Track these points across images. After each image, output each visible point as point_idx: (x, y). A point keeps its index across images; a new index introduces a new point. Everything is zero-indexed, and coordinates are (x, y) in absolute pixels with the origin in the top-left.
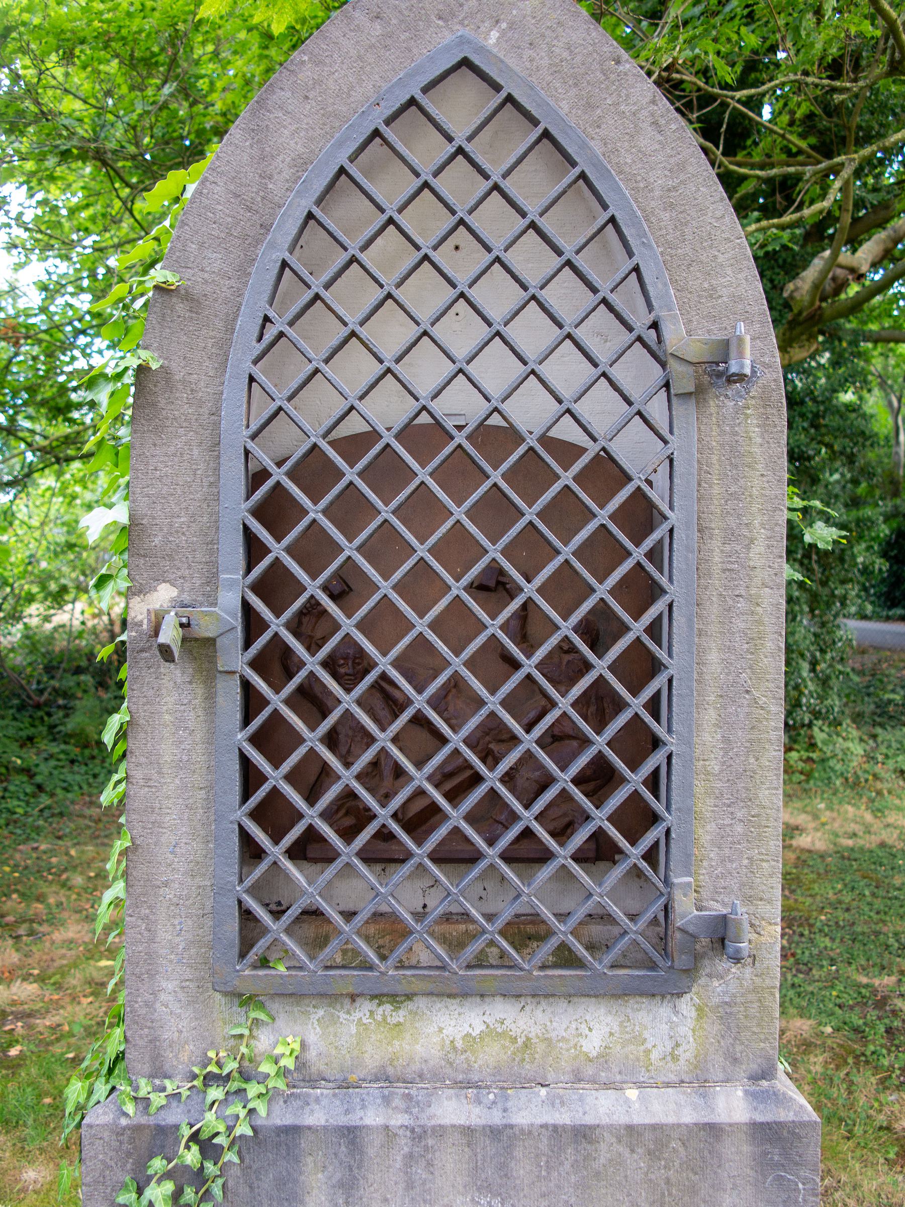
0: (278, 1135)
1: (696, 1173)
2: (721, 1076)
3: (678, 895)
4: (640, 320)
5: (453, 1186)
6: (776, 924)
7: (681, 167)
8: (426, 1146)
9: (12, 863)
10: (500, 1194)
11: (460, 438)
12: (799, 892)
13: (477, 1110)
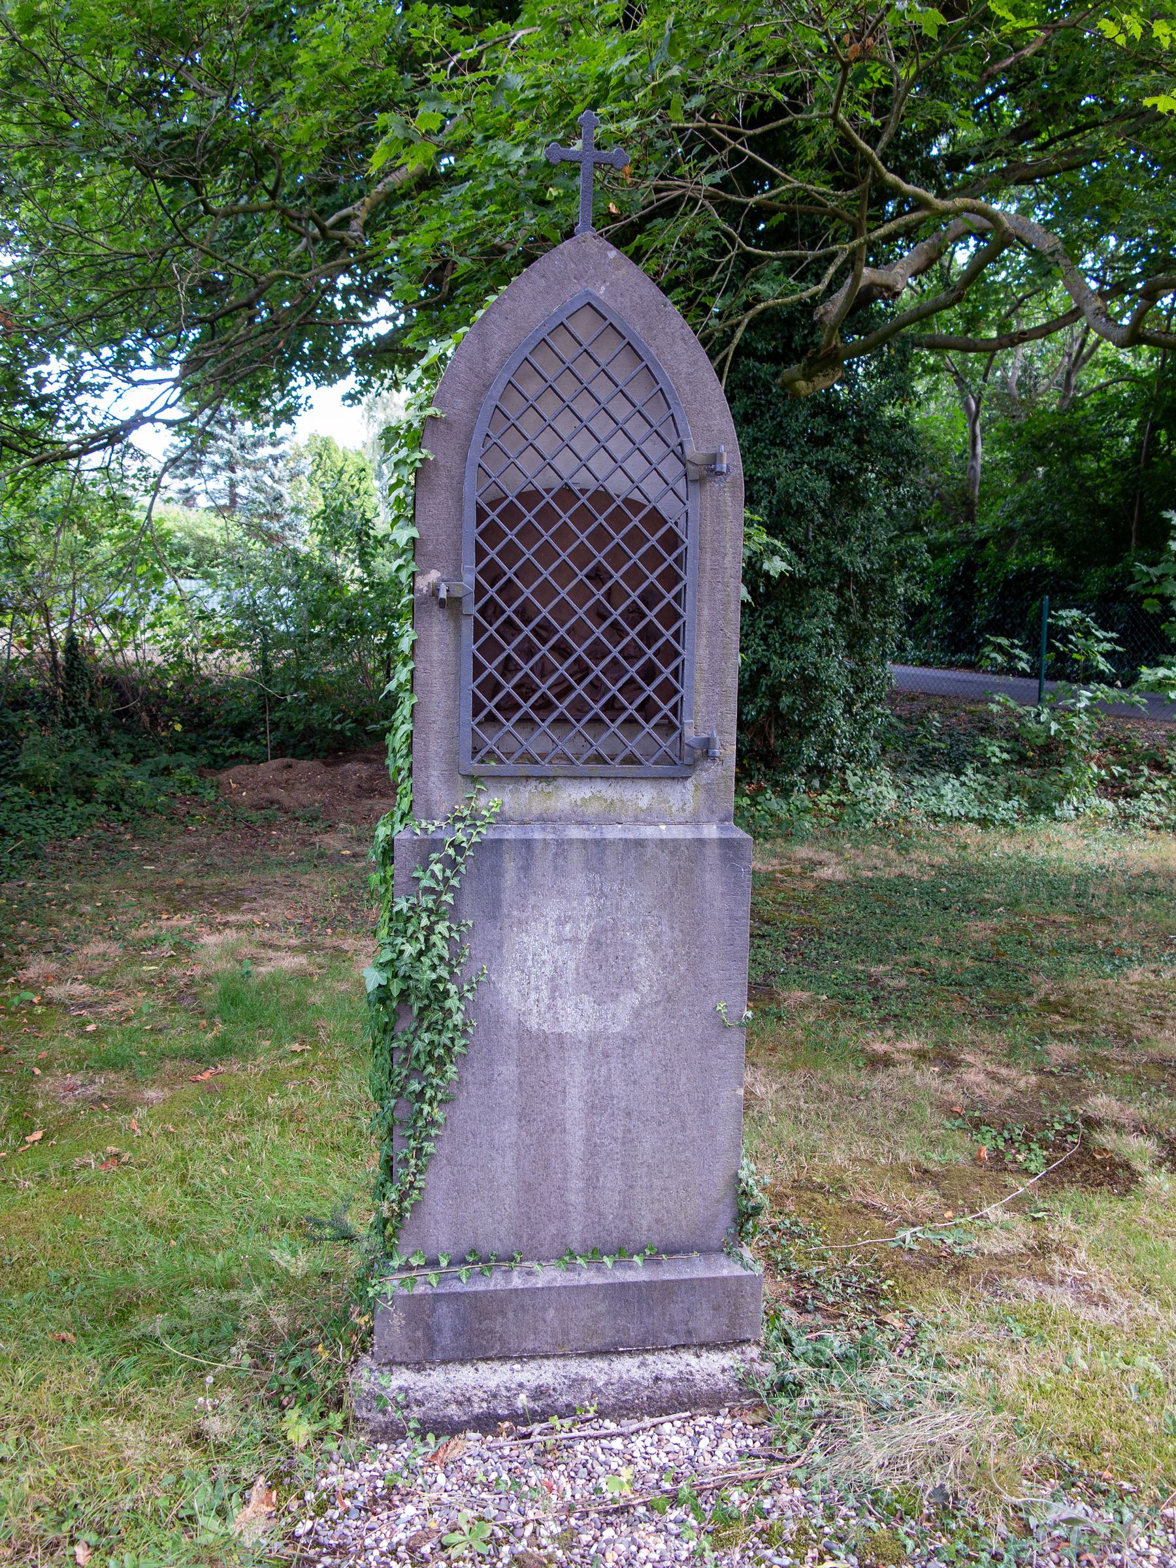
3: (686, 728)
4: (673, 441)
7: (695, 362)
11: (584, 499)
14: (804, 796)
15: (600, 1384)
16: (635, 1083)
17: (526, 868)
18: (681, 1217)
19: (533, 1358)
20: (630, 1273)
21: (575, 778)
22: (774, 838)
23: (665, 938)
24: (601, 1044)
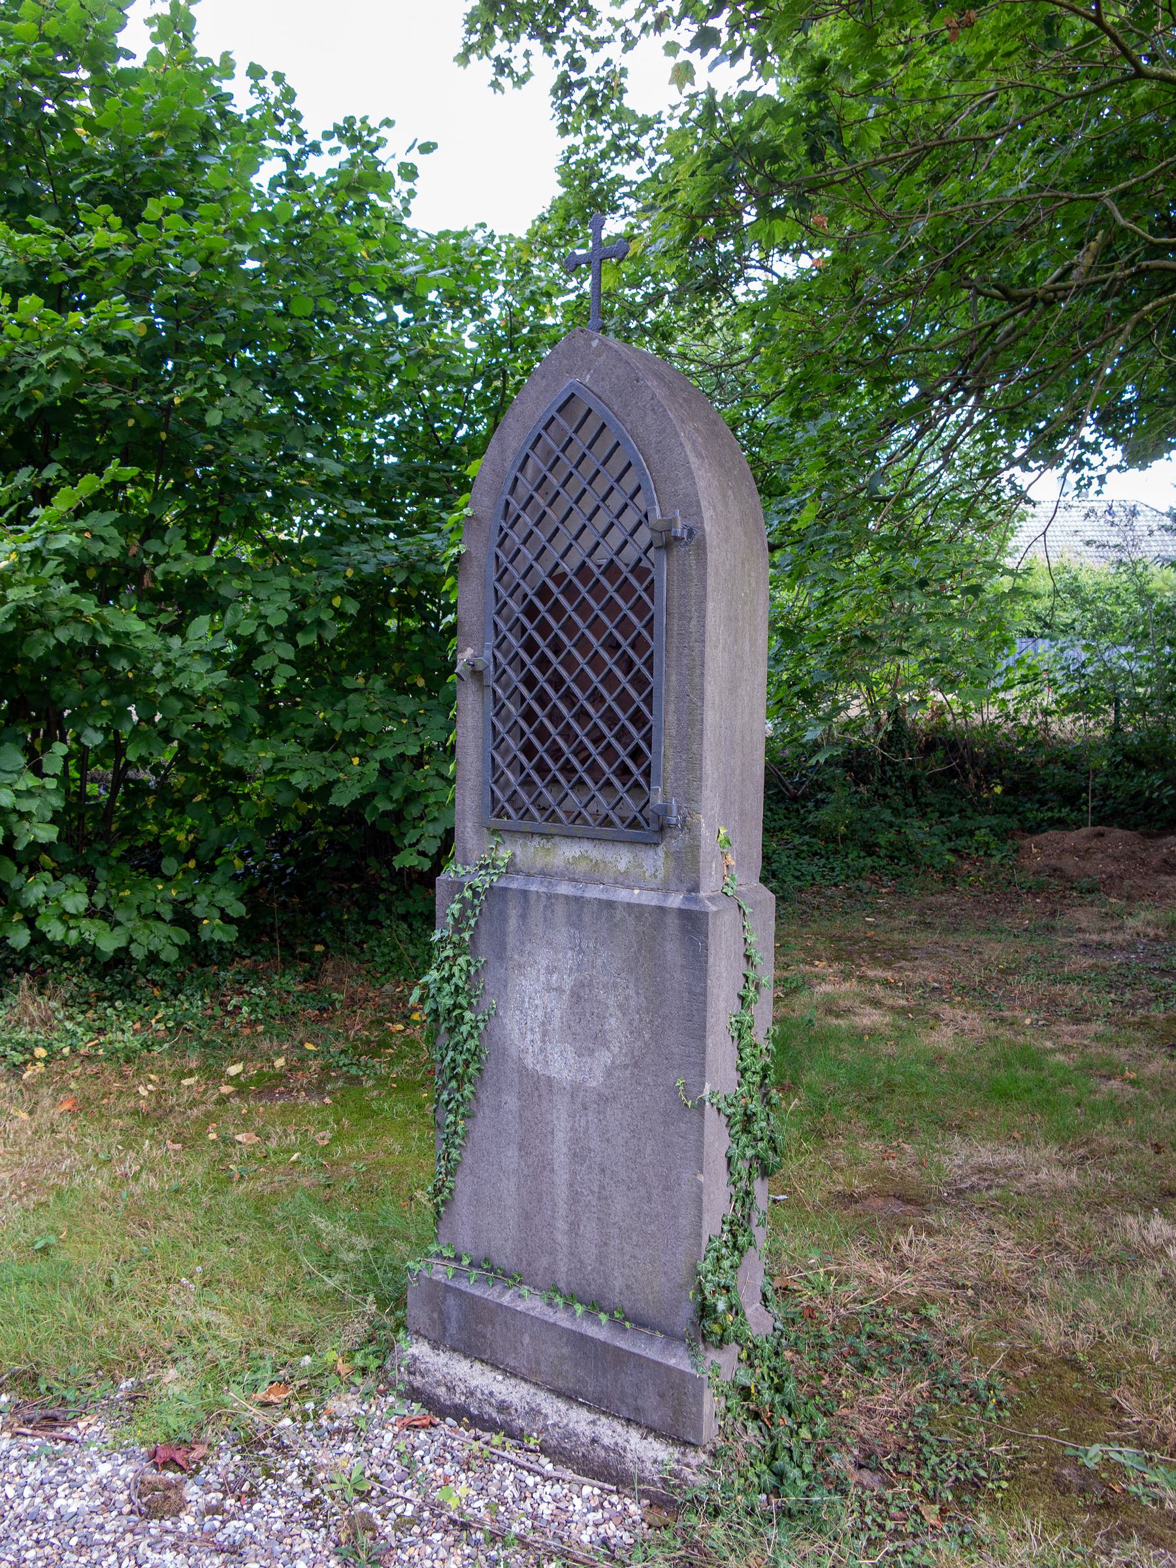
17: (523, 917)
19: (516, 1376)
23: (632, 1003)
24: (581, 1094)
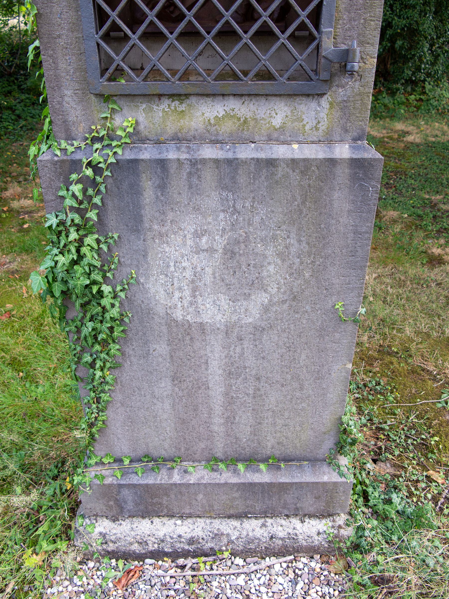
0: (128, 164)
1: (323, 182)
2: (339, 139)
3: (325, 38)
5: (210, 187)
6: (374, 58)
8: (197, 169)
9: (11, 151)
10: (232, 191)
12: (403, 160)
13: (221, 152)
14: (402, 96)
15: (233, 538)
16: (263, 358)
18: (297, 441)
20: (257, 475)
21: (208, 95)
22: (385, 118)
23: (293, 250)
24: (236, 330)
